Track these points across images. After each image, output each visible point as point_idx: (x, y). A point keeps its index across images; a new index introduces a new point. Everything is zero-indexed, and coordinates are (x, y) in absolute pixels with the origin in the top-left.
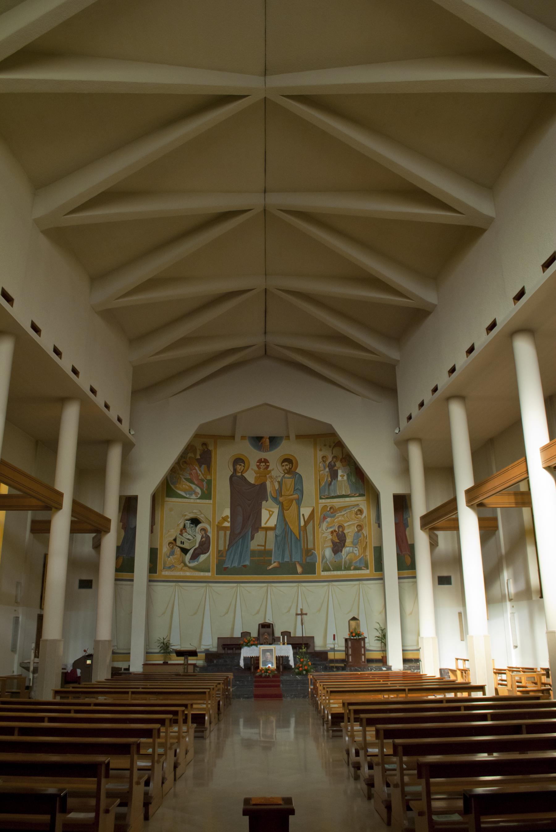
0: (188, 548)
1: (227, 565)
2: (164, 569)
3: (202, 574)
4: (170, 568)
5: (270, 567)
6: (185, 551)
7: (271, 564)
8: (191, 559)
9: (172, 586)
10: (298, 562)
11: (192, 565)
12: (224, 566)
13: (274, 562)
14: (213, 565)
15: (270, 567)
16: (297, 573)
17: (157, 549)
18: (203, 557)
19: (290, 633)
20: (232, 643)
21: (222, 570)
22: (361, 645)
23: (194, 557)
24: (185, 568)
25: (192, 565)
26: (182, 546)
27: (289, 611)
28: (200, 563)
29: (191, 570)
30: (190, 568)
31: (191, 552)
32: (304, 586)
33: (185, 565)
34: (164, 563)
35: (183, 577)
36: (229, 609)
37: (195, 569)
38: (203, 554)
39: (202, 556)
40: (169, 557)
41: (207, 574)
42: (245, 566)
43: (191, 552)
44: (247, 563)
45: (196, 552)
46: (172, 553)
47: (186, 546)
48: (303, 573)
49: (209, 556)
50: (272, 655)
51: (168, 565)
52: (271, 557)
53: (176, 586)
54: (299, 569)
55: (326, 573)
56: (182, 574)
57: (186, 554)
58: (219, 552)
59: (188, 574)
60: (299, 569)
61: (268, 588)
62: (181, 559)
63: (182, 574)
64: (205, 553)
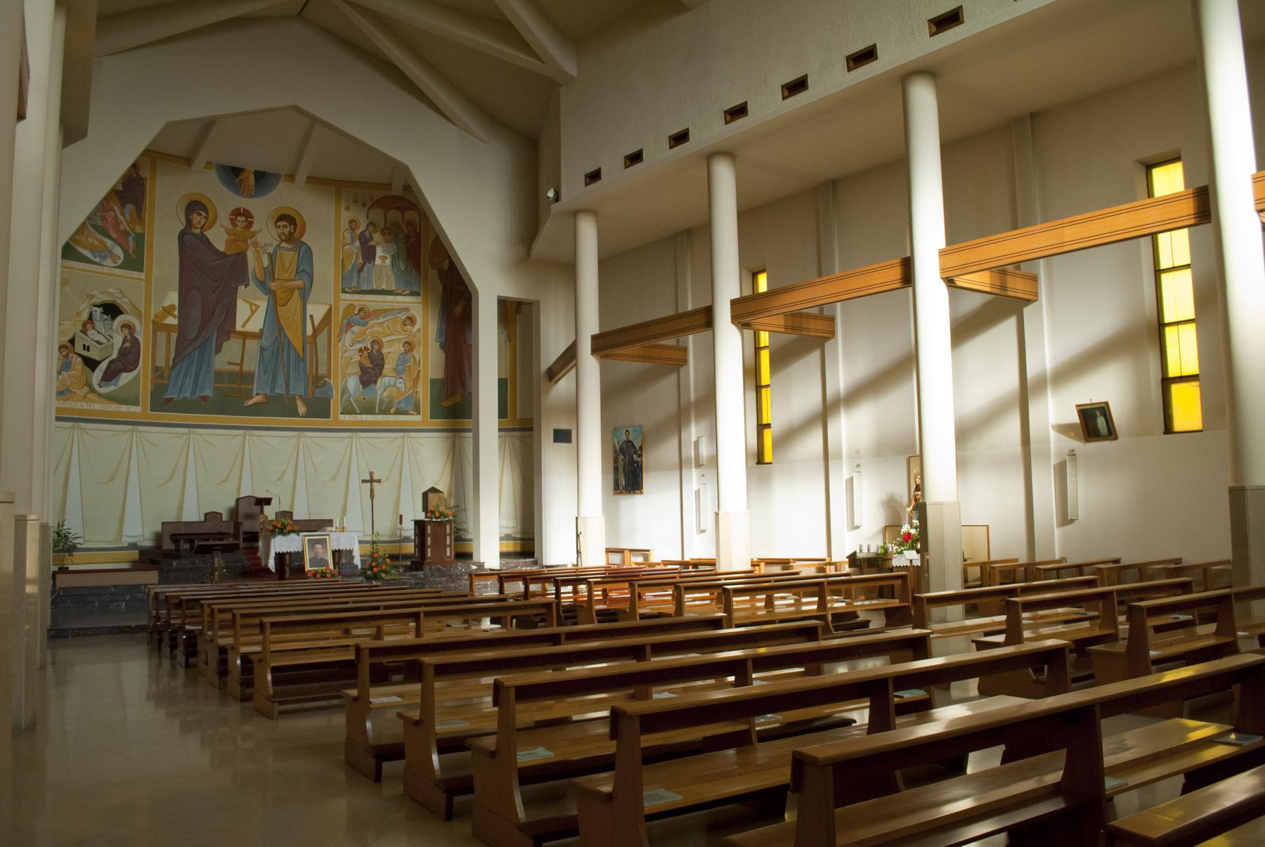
0: (98, 359)
1: (172, 394)
3: (123, 408)
5: (251, 402)
6: (91, 364)
7: (251, 397)
11: (104, 390)
14: (145, 393)
15: (251, 402)
16: (297, 415)
18: (125, 378)
21: (161, 402)
23: (109, 376)
25: (104, 390)
26: (85, 353)
30: (100, 395)
31: (104, 365)
33: (92, 390)
37: (110, 398)
39: (124, 375)
41: (133, 409)
42: (204, 398)
43: (104, 365)
44: (208, 392)
48: (306, 416)
49: (137, 377)
54: (302, 409)
55: (347, 417)
56: (85, 406)
59: (97, 407)
60: (302, 409)
63: (85, 406)
64: (131, 371)
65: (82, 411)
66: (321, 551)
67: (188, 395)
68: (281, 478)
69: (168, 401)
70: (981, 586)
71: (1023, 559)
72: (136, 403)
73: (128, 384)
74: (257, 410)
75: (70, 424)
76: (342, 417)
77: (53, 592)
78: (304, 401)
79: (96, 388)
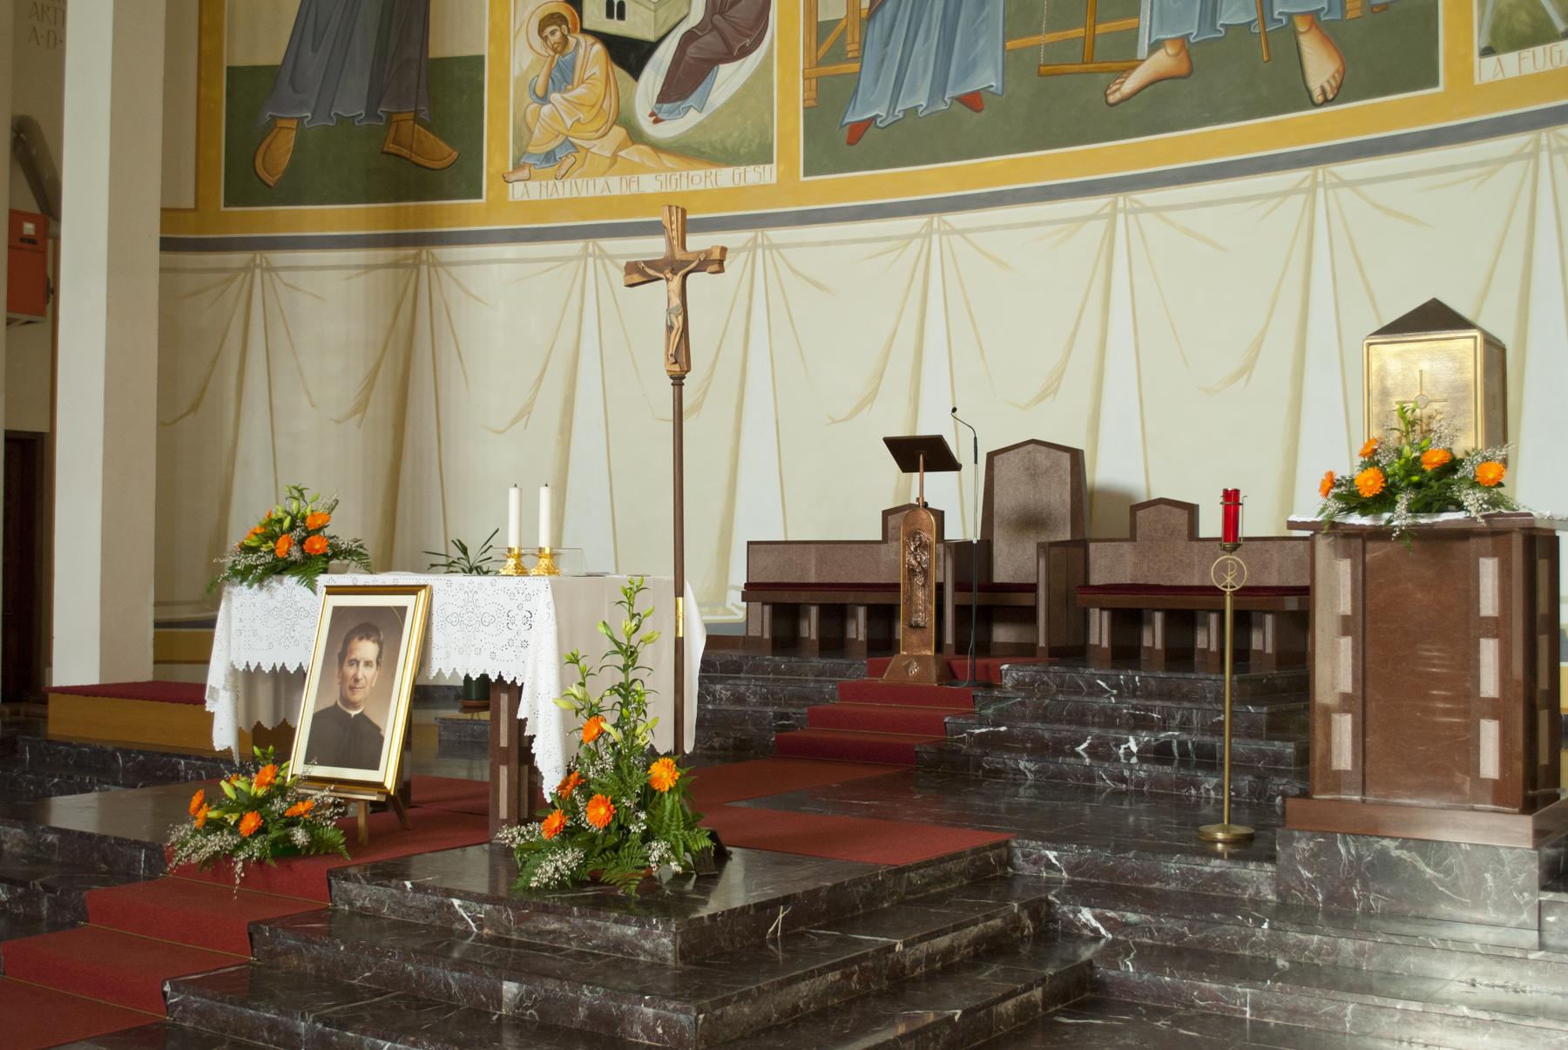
0: (651, 37)
1: (872, 106)
2: (518, 166)
3: (726, 177)
4: (549, 157)
5: (1130, 84)
6: (629, 55)
7: (1132, 64)
8: (663, 97)
9: (564, 260)
10: (1313, 17)
11: (670, 130)
12: (852, 118)
13: (1155, 47)
14: (788, 125)
15: (1130, 84)
16: (1299, 97)
17: (479, 60)
18: (729, 78)
19: (1192, 510)
20: (821, 581)
21: (839, 139)
22: (1471, 596)
23: (684, 83)
24: (634, 153)
25: (670, 130)
26: (614, 27)
27: (1246, 369)
28: (718, 112)
29: (667, 160)
30: (658, 148)
31: (665, 55)
32: (1352, 184)
33: (635, 135)
34: (518, 138)
35: (625, 202)
36: (880, 375)
37: (687, 151)
38: (731, 56)
39: (724, 70)
40: (544, 99)
41: (754, 175)
42: (973, 101)
43: (665, 55)
44: (987, 78)
45: (691, 50)
46: (562, 76)
47: (636, 25)
48: (1342, 92)
49: (765, 67)
50: (387, 660)
51: (538, 146)
52: (1136, 13)
53: (585, 255)
54: (1320, 68)
55: (1513, 64)
56: (616, 186)
57: (635, 71)
58: (820, 30)
59: (649, 184)
60: (1320, 68)
61: (1112, 228)
62: (609, 104)
63: (616, 186)
64: (745, 52)
65: (605, 203)
66: (367, 674)
67: (921, 99)
68: (1246, 369)
69: (858, 131)
70: (1222, 613)
71: (743, 633)
72: (762, 155)
73: (737, 99)
74: (1157, 110)
75: (574, 247)
76: (1488, 70)
77: (120, 842)
78: (1332, 35)
79: (645, 123)
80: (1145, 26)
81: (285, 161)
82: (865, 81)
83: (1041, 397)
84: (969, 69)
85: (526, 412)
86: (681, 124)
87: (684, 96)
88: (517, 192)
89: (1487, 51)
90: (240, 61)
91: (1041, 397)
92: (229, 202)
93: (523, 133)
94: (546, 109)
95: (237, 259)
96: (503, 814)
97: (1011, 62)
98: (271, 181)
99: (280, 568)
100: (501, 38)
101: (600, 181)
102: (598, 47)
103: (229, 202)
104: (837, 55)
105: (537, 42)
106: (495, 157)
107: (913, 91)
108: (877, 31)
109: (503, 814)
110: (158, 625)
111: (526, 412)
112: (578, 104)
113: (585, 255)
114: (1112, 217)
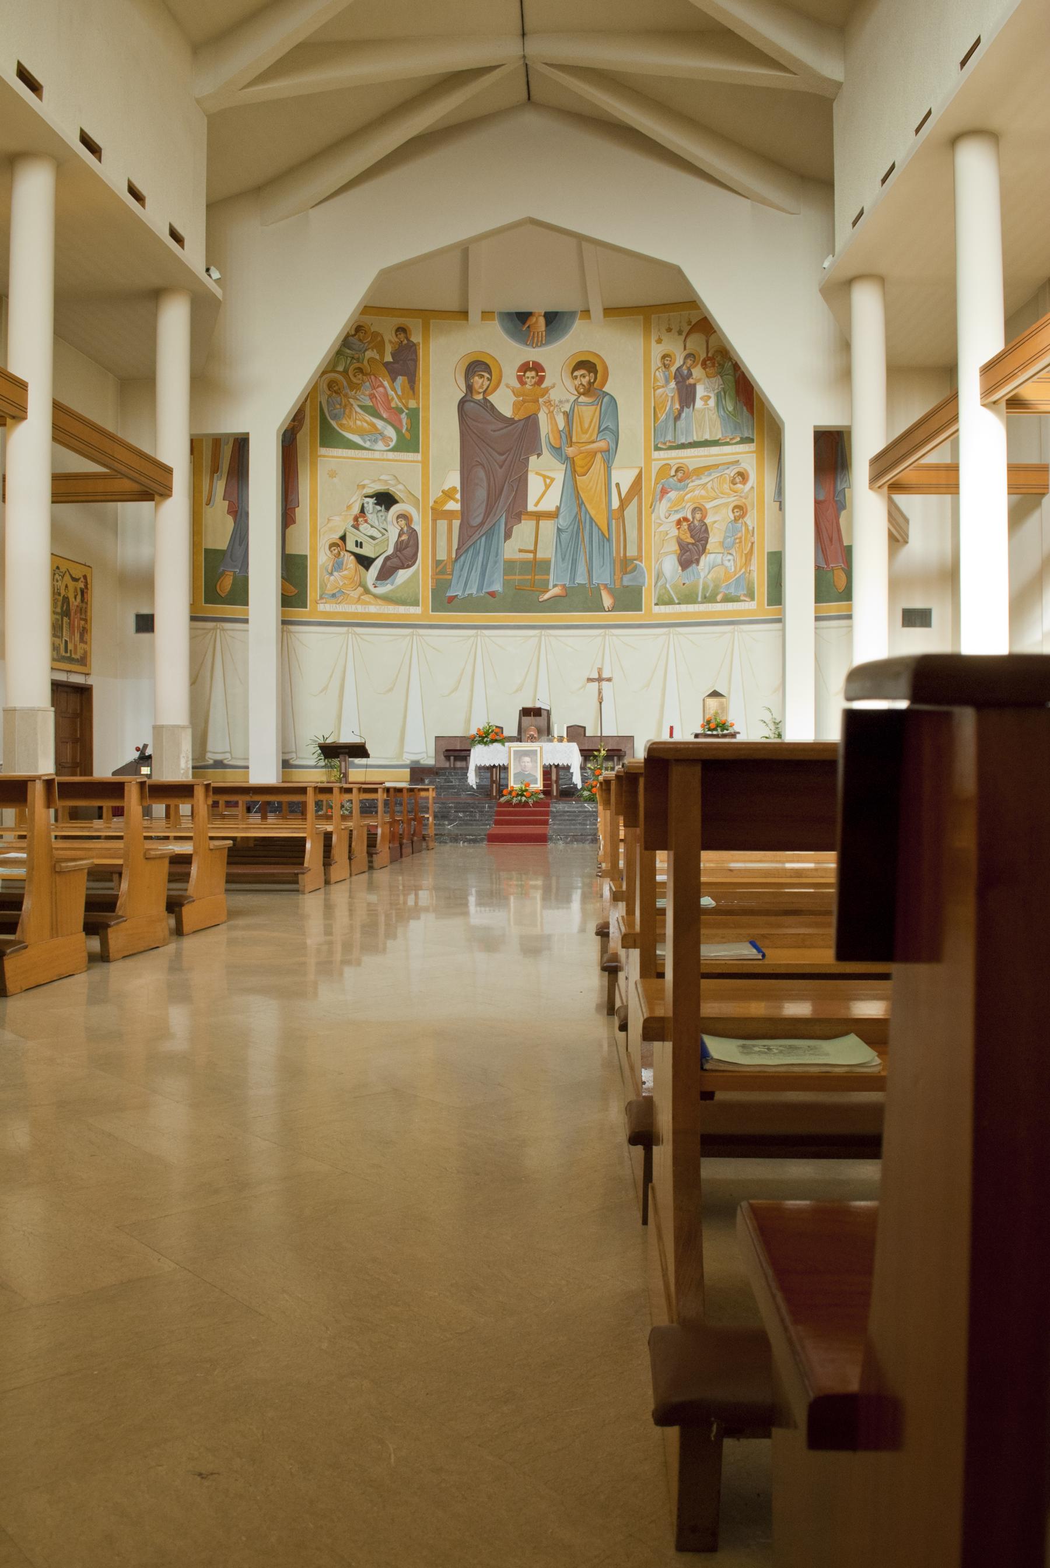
0: (373, 556)
2: (321, 598)
3: (402, 610)
4: (334, 595)
5: (547, 596)
6: (365, 562)
10: (606, 585)
13: (555, 586)
16: (602, 609)
17: (306, 556)
18: (402, 576)
23: (385, 574)
24: (366, 598)
26: (358, 550)
30: (375, 596)
33: (367, 591)
36: (459, 681)
37: (387, 599)
38: (403, 568)
39: (401, 572)
40: (331, 574)
41: (412, 610)
42: (492, 594)
44: (497, 587)
45: (388, 563)
47: (367, 551)
53: (348, 633)
54: (607, 601)
56: (360, 609)
57: (367, 568)
59: (373, 609)
60: (607, 601)
64: (409, 567)
65: (355, 615)
67: (474, 591)
69: (451, 599)
74: (554, 605)
75: (345, 629)
76: (656, 609)
78: (611, 592)
80: (552, 579)
81: (228, 588)
82: (454, 582)
83: (517, 691)
84: (490, 584)
85: (325, 688)
86: (384, 589)
87: (386, 579)
88: (321, 607)
89: (656, 604)
90: (210, 547)
91: (517, 691)
92: (206, 602)
93: (323, 586)
94: (332, 578)
95: (210, 625)
96: (642, 781)
97: (506, 583)
98: (223, 595)
99: (494, 741)
100: (314, 549)
101: (354, 606)
102: (352, 557)
103: (206, 602)
104: (443, 572)
105: (328, 552)
106: (312, 594)
107: (471, 588)
108: (458, 566)
109: (642, 781)
110: (193, 768)
111: (325, 688)
112: (344, 577)
113: (348, 633)
114: (540, 637)
